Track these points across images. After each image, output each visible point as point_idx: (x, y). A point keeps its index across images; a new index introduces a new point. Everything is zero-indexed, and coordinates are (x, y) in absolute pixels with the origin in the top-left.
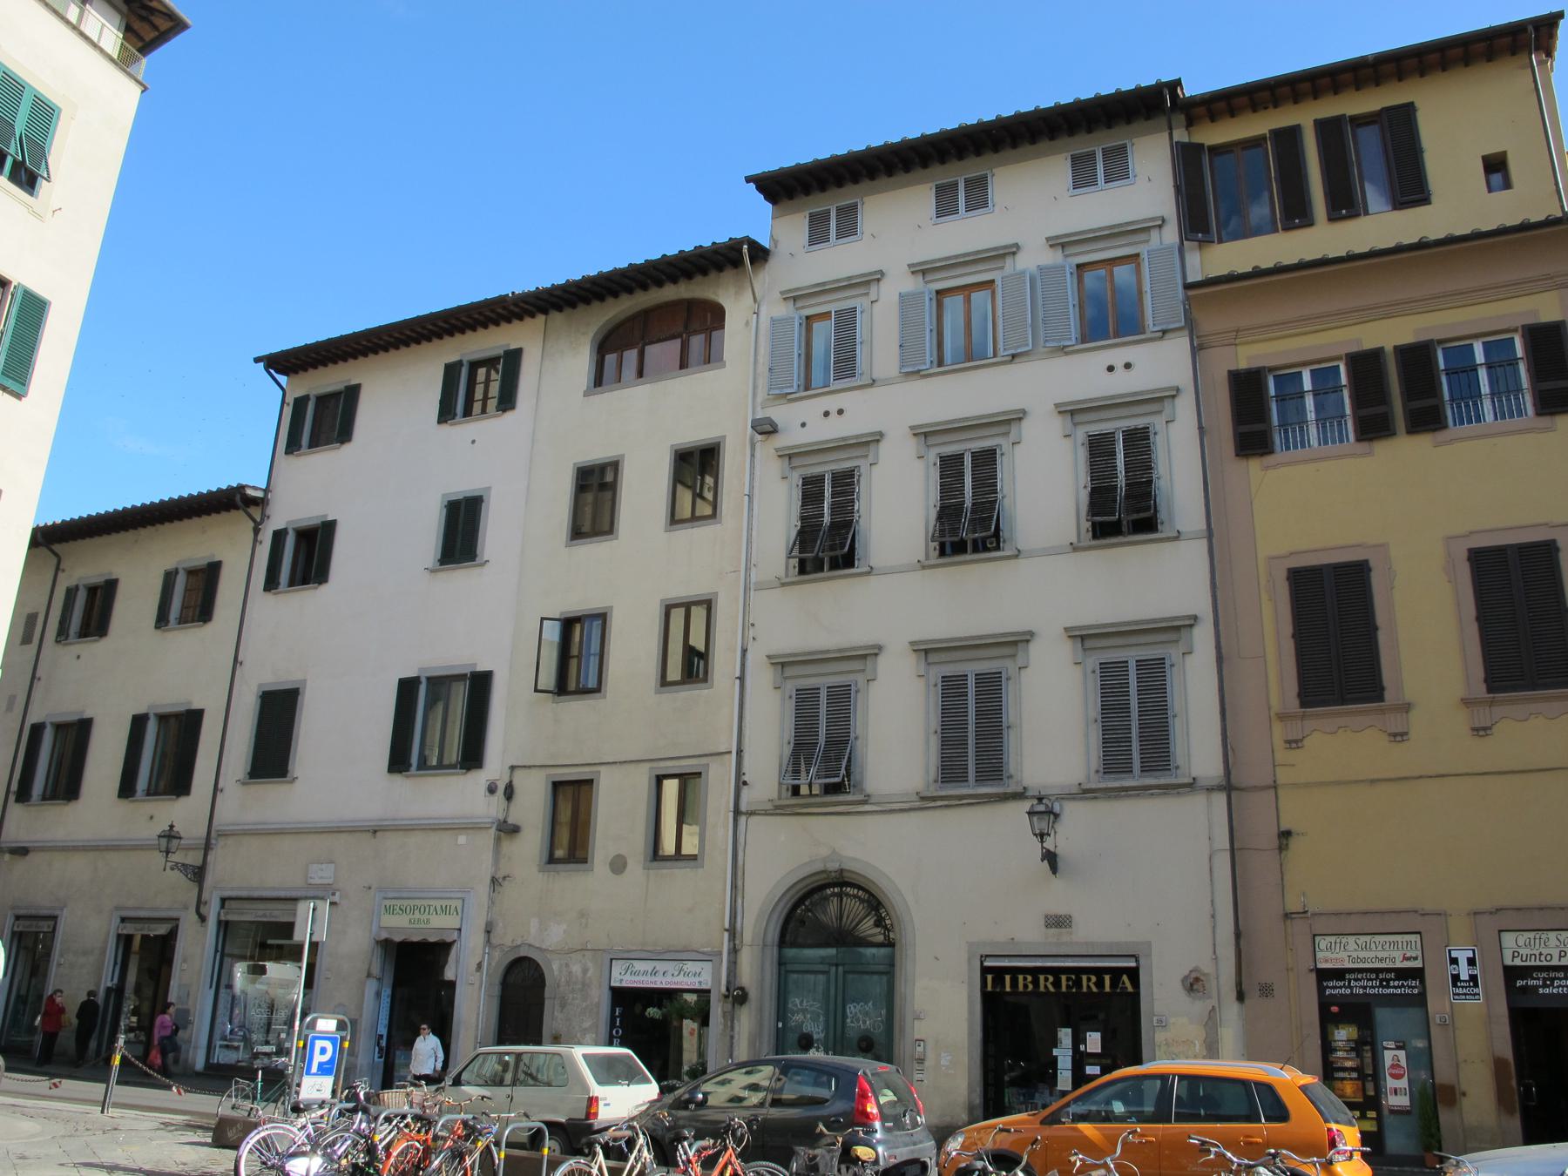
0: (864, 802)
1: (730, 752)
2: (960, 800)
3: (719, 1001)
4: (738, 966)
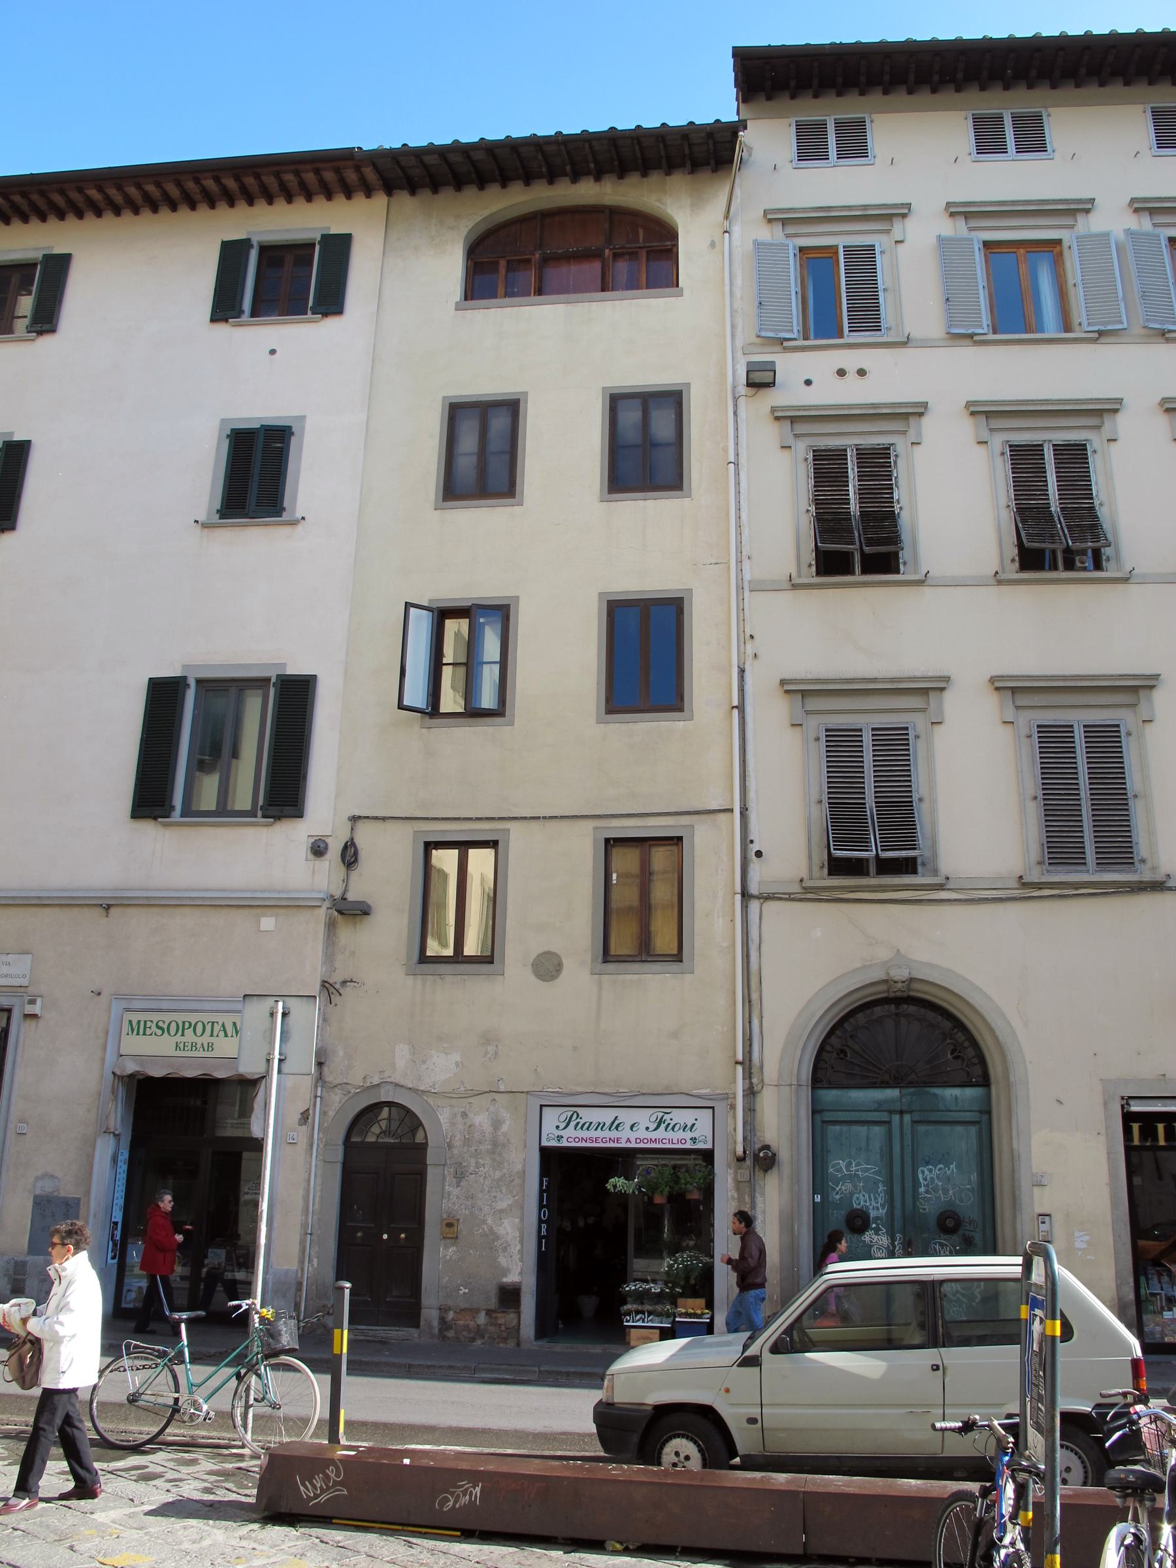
0: (940, 887)
1: (731, 810)
2: (1077, 889)
3: (729, 1166)
4: (758, 1114)
